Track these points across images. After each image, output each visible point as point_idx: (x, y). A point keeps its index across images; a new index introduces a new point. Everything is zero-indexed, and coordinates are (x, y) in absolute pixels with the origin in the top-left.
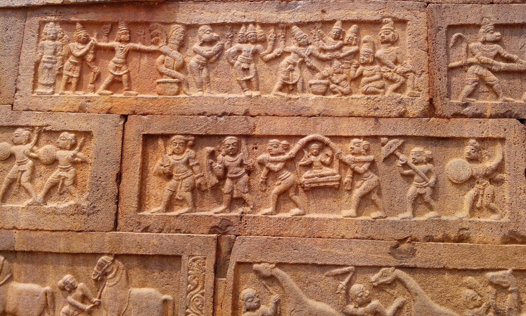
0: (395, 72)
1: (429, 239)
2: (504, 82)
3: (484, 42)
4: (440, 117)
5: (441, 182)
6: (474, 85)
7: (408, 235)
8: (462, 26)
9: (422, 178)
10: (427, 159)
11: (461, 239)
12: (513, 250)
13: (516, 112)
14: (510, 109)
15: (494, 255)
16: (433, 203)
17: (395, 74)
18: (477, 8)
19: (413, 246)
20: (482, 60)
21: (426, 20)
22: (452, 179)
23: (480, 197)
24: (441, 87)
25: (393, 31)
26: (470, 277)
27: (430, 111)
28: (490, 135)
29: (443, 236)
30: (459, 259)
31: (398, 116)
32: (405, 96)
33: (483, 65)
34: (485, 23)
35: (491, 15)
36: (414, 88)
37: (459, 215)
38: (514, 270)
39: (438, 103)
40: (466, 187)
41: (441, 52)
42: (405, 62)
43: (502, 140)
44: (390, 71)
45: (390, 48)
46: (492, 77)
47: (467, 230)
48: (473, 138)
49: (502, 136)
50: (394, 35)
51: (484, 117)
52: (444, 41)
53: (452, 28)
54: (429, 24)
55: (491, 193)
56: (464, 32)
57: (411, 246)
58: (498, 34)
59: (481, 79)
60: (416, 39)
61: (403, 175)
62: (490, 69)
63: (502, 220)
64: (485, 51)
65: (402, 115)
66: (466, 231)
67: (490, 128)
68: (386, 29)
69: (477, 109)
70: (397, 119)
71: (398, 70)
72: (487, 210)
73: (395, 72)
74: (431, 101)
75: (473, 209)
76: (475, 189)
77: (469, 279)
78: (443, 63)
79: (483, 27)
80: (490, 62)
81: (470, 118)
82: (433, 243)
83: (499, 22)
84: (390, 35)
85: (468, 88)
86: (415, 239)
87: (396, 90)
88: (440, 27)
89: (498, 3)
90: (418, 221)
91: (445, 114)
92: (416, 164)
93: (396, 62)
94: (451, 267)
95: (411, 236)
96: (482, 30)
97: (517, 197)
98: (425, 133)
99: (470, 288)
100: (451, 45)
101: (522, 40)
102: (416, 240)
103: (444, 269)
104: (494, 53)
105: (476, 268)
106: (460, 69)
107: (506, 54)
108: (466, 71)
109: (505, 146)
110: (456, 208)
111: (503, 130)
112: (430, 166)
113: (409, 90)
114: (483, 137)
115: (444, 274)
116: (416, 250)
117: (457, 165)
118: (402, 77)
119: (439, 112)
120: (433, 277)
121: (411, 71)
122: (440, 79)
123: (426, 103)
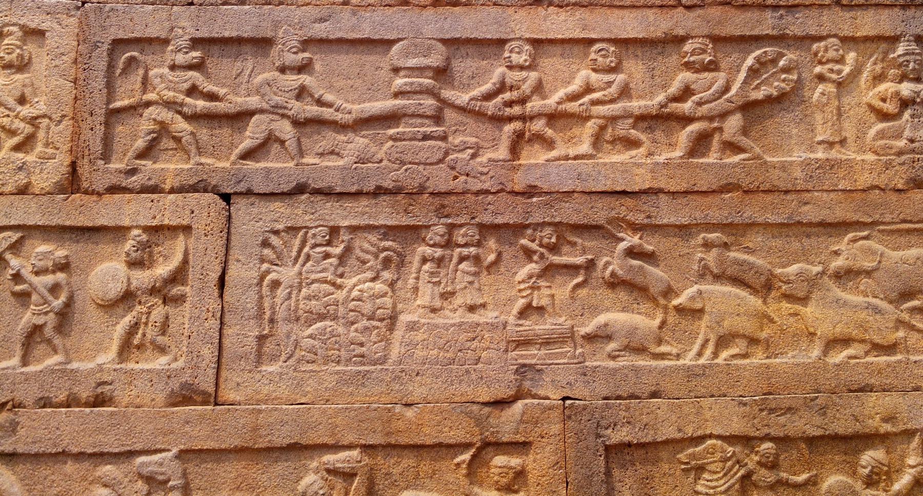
0: (16, 117)
1: (45, 403)
2: (204, 134)
3: (173, 67)
4: (86, 192)
5: (78, 305)
6: (149, 138)
7: (9, 398)
8: (137, 41)
9: (43, 297)
10: (55, 265)
11: (99, 401)
12: (183, 417)
13: (213, 183)
14: (205, 177)
15: (151, 426)
16: (57, 341)
17: (17, 121)
18: (163, 12)
19: (14, 417)
20: (165, 98)
21: (76, 31)
22: (95, 298)
23: (142, 326)
24: (91, 141)
25: (18, 47)
26: (109, 467)
27: (72, 183)
28: (166, 222)
29: (69, 396)
30: (90, 436)
31: (15, 191)
32: (31, 158)
33: (169, 104)
34: (176, 37)
35: (187, 23)
36: (47, 145)
37: (101, 359)
38: (181, 451)
39: (84, 169)
40: (120, 311)
41: (98, 83)
42: (36, 100)
43: (187, 229)
44: (8, 116)
45: (12, 77)
46: (181, 126)
47: (111, 384)
48: (137, 227)
49: (185, 223)
50: (21, 56)
51: (161, 191)
52: (103, 65)
53: (118, 44)
54: (81, 38)
55: (160, 319)
56: (142, 52)
57: (12, 416)
58: (196, 54)
59: (163, 129)
60: (57, 62)
61: (15, 294)
62: (179, 113)
63: (174, 365)
64: (171, 82)
65: (23, 191)
66: (108, 387)
67: (169, 210)
68: (8, 45)
69: (149, 179)
70: (13, 197)
71: (21, 114)
72: (153, 350)
73: (16, 117)
74: (73, 165)
75: (126, 348)
76: (134, 313)
77: (108, 470)
78: (98, 102)
79: (172, 42)
80: (179, 101)
81: (138, 193)
82: (49, 410)
83: (199, 35)
84: (14, 55)
85: (140, 144)
86: (20, 404)
87: (17, 148)
88: (99, 42)
89: (201, 5)
90: (27, 373)
91: (94, 187)
92: (37, 273)
93: (22, 100)
94: (75, 450)
95: (13, 400)
96: (170, 48)
97: (201, 325)
98: (55, 221)
99: (105, 486)
100: (118, 71)
101: (239, 64)
102: (20, 405)
103: (63, 455)
104: (186, 86)
105: (117, 450)
106: (132, 111)
107: (209, 87)
108: (141, 116)
109: (192, 240)
110: (100, 347)
111: (188, 212)
112: (61, 276)
113: (39, 148)
114: (153, 224)
115: (66, 463)
116: (18, 423)
117: (108, 272)
118: (27, 126)
119: (85, 185)
120: (45, 469)
121: (44, 116)
122: (92, 129)
123: (65, 169)
